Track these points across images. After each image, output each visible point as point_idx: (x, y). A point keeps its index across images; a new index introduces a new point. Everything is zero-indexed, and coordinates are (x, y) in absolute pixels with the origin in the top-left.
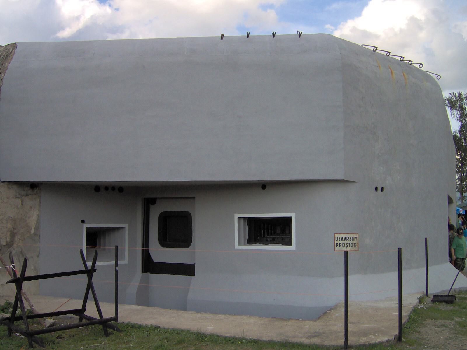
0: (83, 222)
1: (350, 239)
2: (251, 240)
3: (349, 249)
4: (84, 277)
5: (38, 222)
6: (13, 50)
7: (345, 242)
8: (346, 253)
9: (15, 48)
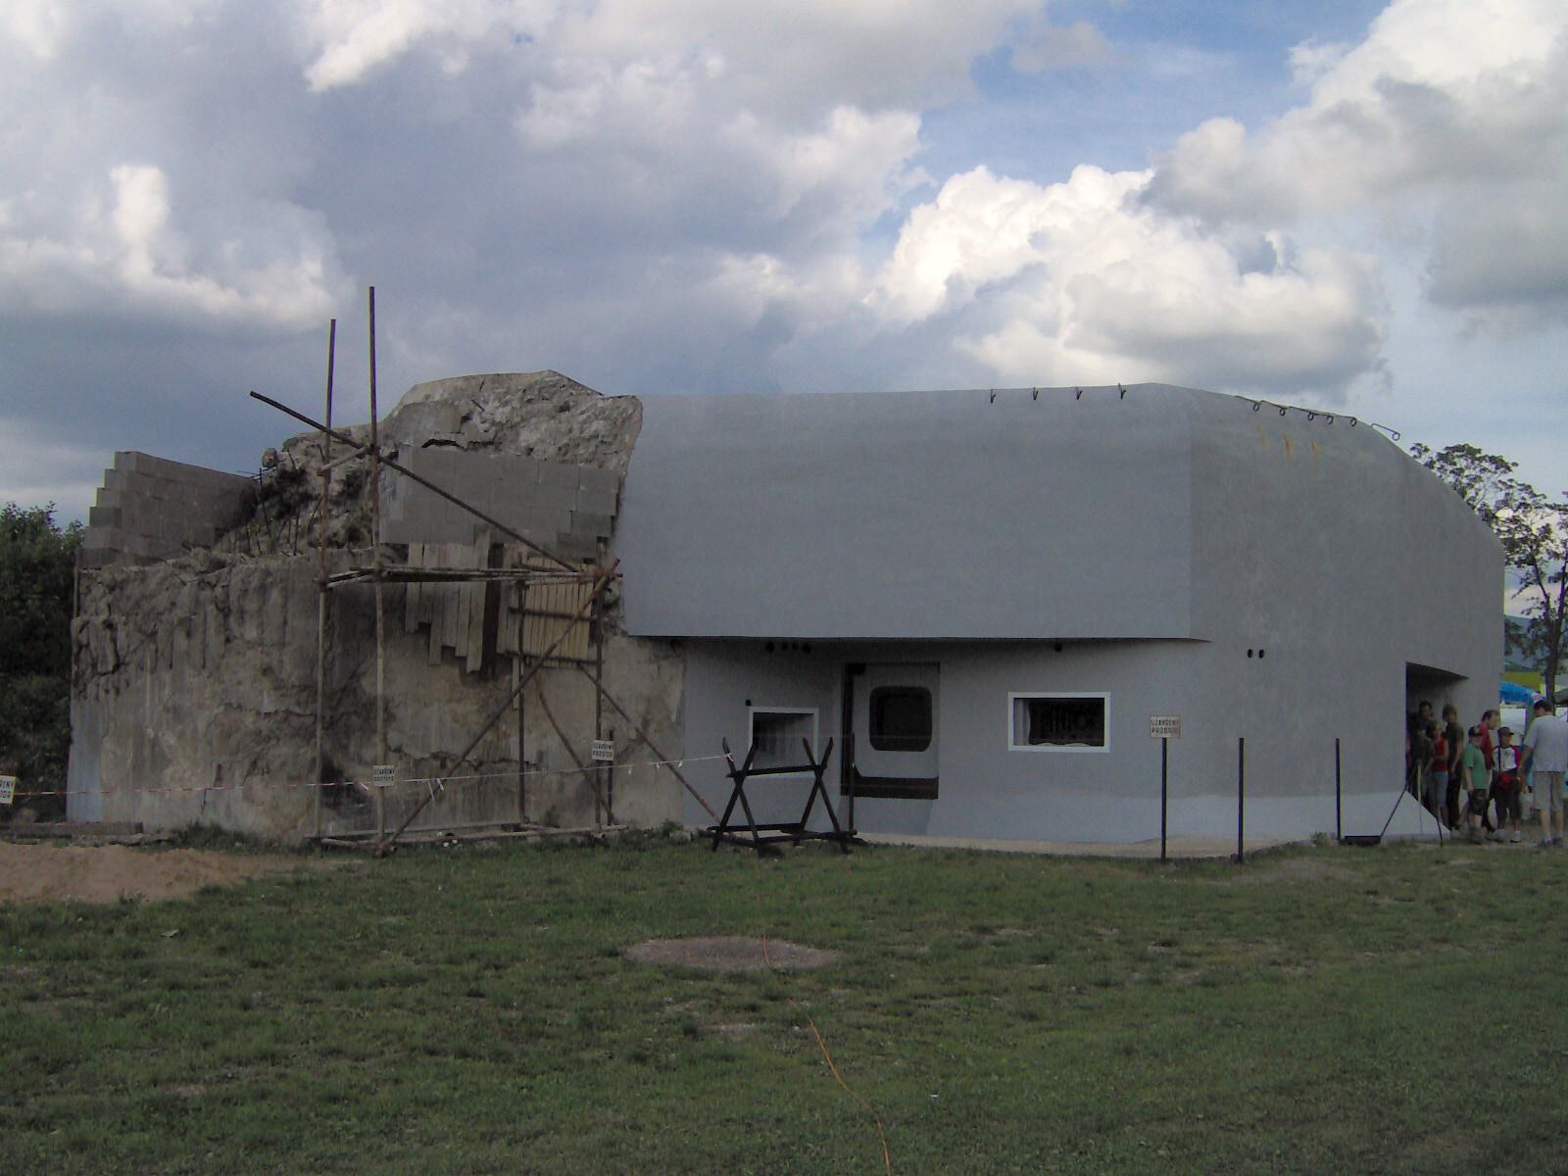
0: (748, 703)
2: (1037, 735)
3: (1167, 736)
4: (812, 775)
5: (682, 703)
8: (1165, 740)
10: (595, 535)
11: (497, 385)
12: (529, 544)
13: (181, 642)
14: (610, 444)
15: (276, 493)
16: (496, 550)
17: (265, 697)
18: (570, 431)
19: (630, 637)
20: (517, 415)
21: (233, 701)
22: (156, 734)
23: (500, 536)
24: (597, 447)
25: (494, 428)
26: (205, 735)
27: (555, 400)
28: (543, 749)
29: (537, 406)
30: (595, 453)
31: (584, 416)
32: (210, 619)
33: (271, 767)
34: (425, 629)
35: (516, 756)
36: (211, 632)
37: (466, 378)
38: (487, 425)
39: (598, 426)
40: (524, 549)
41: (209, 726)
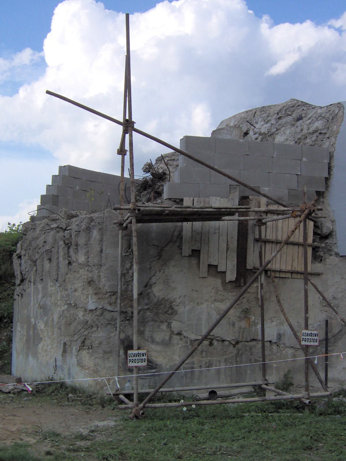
1: (141, 355)
6: (339, 112)
7: (309, 337)
9: (342, 108)
10: (314, 189)
11: (263, 113)
12: (267, 197)
13: (47, 265)
14: (325, 133)
15: (150, 186)
16: (244, 199)
17: (90, 299)
18: (302, 130)
19: (341, 256)
20: (274, 128)
21: (72, 302)
22: (35, 322)
23: (248, 192)
24: (317, 137)
25: (261, 137)
26: (58, 322)
27: (294, 115)
28: (282, 332)
29: (283, 121)
30: (316, 140)
31: (310, 121)
32: (61, 250)
33: (93, 345)
34: (196, 253)
35: (260, 337)
36: (61, 259)
37: (247, 112)
38: (257, 136)
39: (318, 124)
40: (264, 200)
41: (59, 317)
